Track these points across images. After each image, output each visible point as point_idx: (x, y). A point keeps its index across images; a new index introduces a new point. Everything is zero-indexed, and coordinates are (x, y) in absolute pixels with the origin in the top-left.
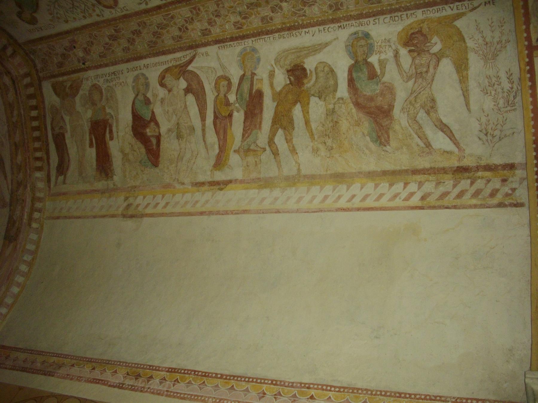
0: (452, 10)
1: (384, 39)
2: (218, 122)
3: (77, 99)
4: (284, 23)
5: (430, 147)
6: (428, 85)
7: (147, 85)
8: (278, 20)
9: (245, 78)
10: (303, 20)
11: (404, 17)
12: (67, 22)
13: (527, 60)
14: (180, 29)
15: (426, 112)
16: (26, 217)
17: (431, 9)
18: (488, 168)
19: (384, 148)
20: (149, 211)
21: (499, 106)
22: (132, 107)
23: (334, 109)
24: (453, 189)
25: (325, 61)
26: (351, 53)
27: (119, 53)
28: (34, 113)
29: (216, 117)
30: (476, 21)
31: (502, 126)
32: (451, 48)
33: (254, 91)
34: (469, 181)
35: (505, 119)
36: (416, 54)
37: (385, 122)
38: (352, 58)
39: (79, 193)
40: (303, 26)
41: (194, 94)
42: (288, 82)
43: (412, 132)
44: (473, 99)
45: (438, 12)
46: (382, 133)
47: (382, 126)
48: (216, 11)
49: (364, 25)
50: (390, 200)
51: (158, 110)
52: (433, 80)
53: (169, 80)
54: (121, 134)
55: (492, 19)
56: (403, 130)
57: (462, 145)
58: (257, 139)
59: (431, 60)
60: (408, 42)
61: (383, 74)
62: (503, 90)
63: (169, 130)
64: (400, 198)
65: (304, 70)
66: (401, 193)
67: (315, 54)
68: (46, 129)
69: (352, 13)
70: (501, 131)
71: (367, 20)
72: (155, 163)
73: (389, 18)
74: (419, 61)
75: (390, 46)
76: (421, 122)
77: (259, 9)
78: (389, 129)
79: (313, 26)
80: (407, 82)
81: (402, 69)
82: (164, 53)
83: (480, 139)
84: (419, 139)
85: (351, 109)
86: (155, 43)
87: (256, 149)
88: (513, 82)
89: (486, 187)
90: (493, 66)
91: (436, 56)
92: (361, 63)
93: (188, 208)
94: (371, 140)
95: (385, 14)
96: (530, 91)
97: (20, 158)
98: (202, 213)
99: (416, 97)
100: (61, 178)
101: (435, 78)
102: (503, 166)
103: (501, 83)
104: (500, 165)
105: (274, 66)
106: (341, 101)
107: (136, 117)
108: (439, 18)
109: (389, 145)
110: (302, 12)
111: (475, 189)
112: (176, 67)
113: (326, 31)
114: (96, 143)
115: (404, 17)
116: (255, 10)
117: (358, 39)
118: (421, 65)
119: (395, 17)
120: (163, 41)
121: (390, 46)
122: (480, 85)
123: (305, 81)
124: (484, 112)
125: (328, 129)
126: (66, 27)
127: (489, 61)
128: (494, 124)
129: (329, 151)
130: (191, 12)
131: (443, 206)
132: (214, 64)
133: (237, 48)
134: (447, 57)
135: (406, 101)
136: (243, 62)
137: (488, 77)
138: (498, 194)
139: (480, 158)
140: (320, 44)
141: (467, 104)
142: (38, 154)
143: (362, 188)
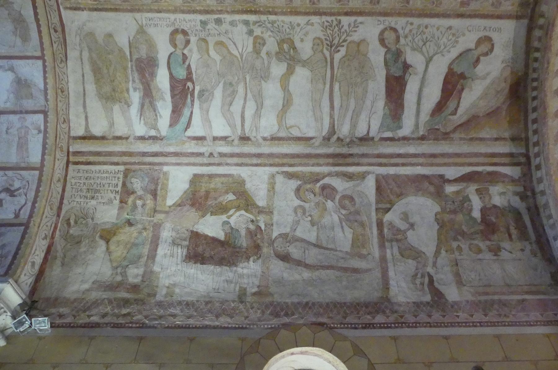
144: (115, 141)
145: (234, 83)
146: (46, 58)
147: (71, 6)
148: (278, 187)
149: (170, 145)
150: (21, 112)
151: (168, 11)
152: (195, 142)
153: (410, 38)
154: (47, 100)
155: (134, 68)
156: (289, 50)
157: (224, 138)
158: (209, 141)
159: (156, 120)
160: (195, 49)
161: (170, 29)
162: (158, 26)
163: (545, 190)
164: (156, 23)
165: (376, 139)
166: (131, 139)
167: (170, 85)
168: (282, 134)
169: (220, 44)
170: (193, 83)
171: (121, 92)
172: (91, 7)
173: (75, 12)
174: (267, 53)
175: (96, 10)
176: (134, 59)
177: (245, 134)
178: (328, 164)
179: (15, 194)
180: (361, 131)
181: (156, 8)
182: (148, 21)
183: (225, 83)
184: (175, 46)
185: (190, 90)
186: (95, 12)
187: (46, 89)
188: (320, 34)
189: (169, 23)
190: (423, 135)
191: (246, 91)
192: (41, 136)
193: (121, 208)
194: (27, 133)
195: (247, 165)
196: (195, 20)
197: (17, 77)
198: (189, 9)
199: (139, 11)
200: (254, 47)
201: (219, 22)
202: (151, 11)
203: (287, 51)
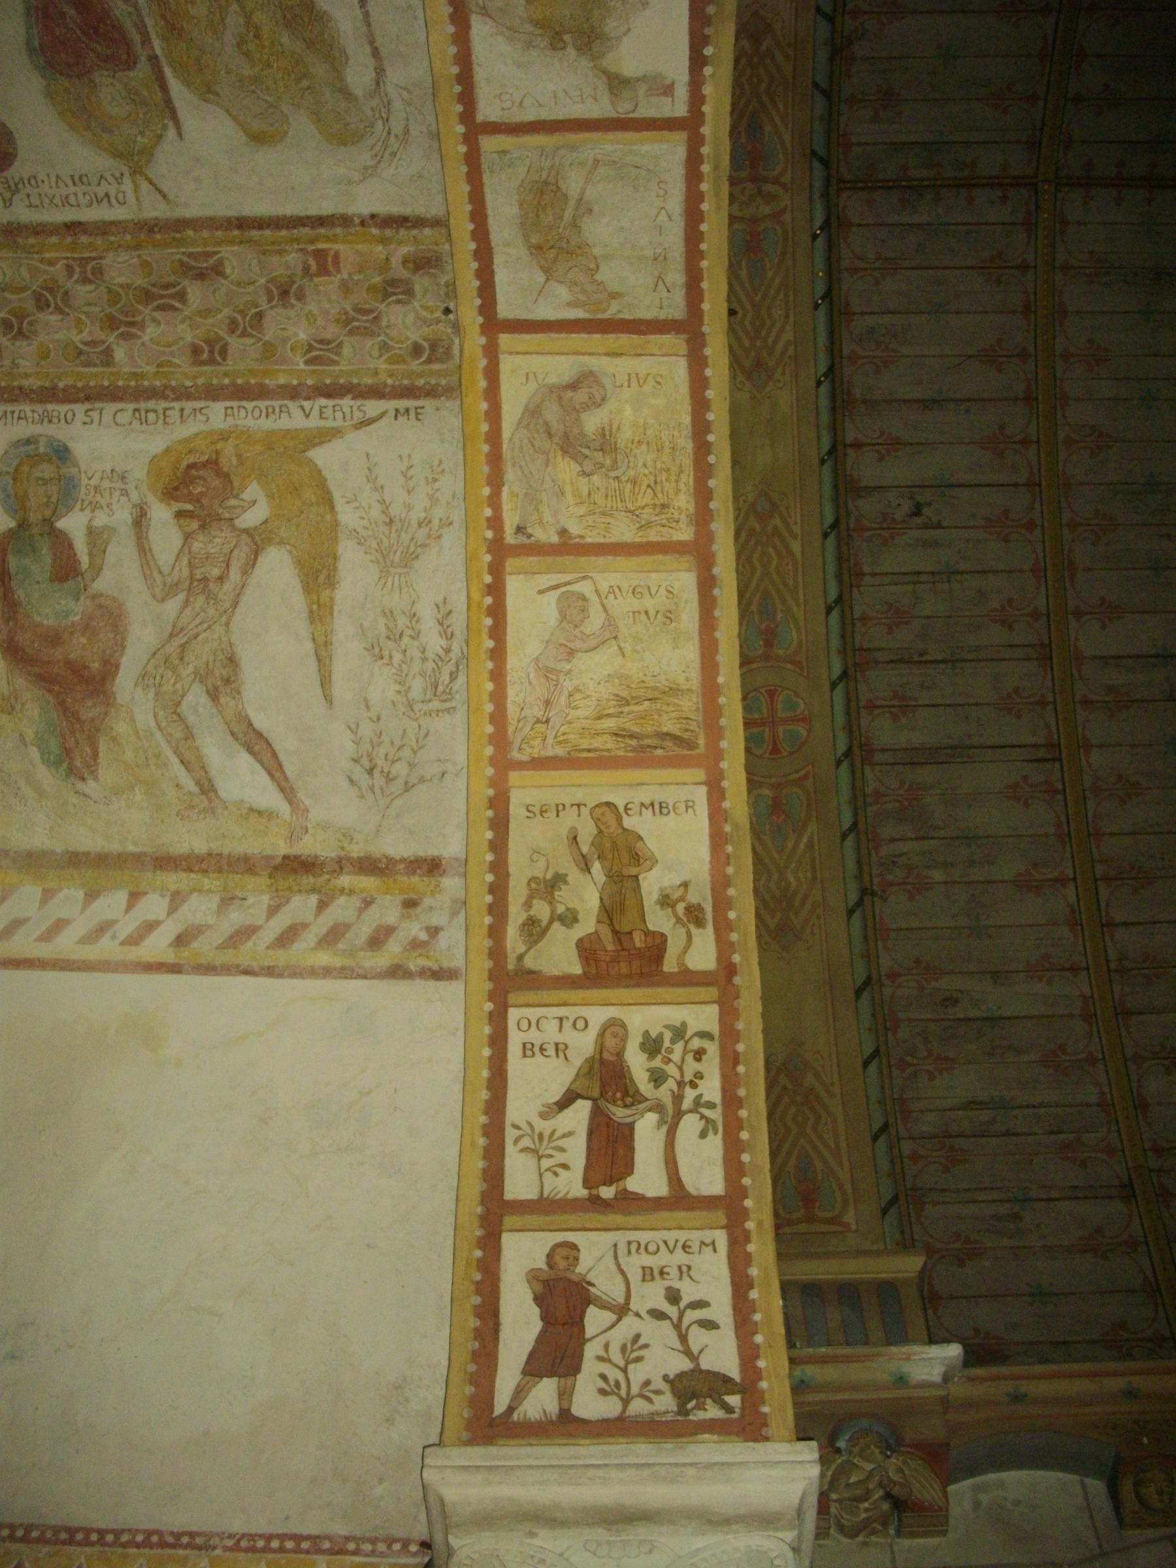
0: (307, 416)
1: (108, 468)
5: (212, 795)
6: (221, 615)
11: (174, 415)
13: (488, 579)
15: (208, 692)
17: (250, 405)
18: (369, 865)
19: (80, 786)
21: (411, 696)
24: (267, 920)
26: (8, 496)
30: (368, 455)
31: (415, 753)
32: (295, 520)
34: (314, 900)
35: (422, 733)
36: (195, 525)
37: (89, 710)
38: (11, 512)
44: (340, 670)
45: (267, 416)
46: (77, 742)
47: (78, 720)
49: (55, 420)
52: (235, 604)
55: (409, 456)
56: (138, 737)
57: (301, 795)
59: (235, 546)
60: (176, 489)
61: (98, 571)
62: (423, 652)
64: (114, 937)
66: (115, 922)
69: (25, 383)
70: (410, 765)
73: (130, 412)
74: (201, 545)
75: (125, 492)
76: (191, 719)
78: (98, 730)
80: (163, 600)
81: (152, 563)
83: (352, 782)
84: (183, 768)
88: (452, 635)
89: (359, 917)
90: (403, 584)
91: (251, 536)
92: (35, 530)
94: (42, 758)
95: (121, 399)
96: (490, 665)
99: (183, 647)
101: (244, 600)
102: (411, 862)
103: (419, 633)
104: (403, 860)
108: (270, 433)
109: (96, 779)
111: (331, 924)
115: (174, 415)
118: (207, 558)
119: (147, 412)
121: (125, 492)
124: (368, 707)
127: (392, 570)
128: (392, 743)
131: (238, 966)
134: (281, 543)
135: (155, 654)
137: (387, 611)
138: (391, 939)
139: (348, 836)
141: (325, 682)
146: (461, 129)
147: (415, 232)
151: (40, 230)
155: (136, 38)
162: (72, 177)
164: (79, 190)
172: (339, 231)
173: (407, 211)
175: (321, 221)
181: (84, 239)
182: (112, 195)
186: (324, 213)
189: (29, 189)
199: (150, 227)
202: (103, 229)
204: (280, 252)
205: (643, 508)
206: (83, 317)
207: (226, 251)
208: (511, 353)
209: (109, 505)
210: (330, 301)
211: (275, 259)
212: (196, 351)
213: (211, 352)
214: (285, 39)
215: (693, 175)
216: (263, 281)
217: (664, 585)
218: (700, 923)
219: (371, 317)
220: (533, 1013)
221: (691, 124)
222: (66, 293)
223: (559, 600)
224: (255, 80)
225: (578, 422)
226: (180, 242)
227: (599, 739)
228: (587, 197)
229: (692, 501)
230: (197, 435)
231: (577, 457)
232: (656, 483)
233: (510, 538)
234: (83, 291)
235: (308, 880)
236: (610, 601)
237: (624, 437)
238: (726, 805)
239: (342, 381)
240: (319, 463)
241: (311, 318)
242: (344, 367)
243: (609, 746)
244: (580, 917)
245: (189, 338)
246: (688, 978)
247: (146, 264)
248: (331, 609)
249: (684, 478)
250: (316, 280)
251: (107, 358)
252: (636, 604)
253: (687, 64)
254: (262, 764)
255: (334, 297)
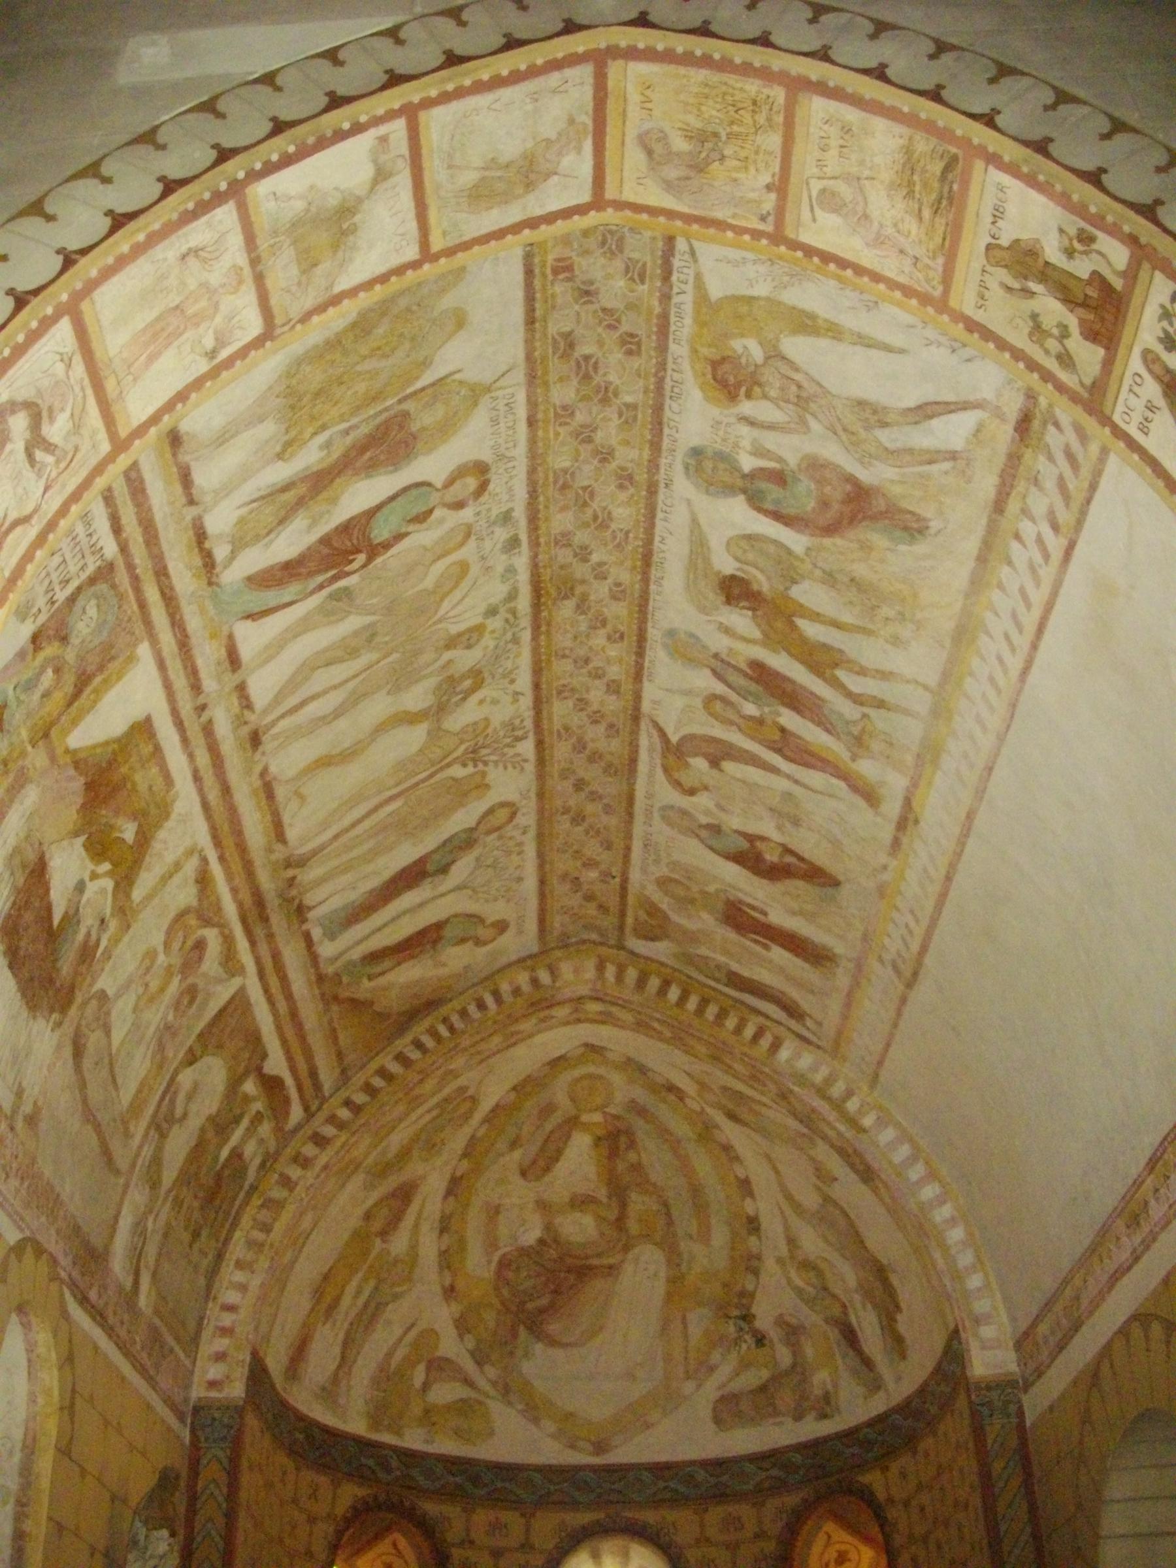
2: (789, 754)
3: (675, 917)
4: (634, 568)
7: (684, 813)
8: (626, 576)
9: (718, 670)
10: (636, 538)
11: (676, 376)
12: (520, 879)
14: (596, 722)
16: (842, 1128)
17: (673, 328)
20: (915, 946)
22: (719, 854)
23: (824, 571)
25: (725, 540)
27: (613, 821)
28: (674, 994)
29: (779, 751)
33: (749, 671)
36: (757, 389)
37: (880, 504)
39: (845, 1017)
40: (649, 541)
41: (723, 759)
42: (750, 613)
43: (911, 469)
48: (575, 662)
50: (1038, 584)
51: (734, 822)
52: (819, 384)
53: (688, 780)
54: (760, 895)
57: (971, 398)
58: (841, 715)
60: (730, 393)
61: (780, 460)
63: (779, 828)
65: (733, 577)
67: (709, 548)
68: (714, 989)
71: (665, 438)
72: (836, 884)
76: (899, 445)
77: (592, 598)
79: (652, 525)
82: (633, 761)
83: (969, 360)
85: (835, 545)
86: (610, 765)
87: (859, 728)
93: (934, 889)
97: (738, 1066)
98: (948, 878)
99: (845, 430)
100: (809, 1022)
105: (709, 618)
106: (814, 554)
107: (738, 858)
109: (930, 520)
110: (620, 535)
112: (664, 757)
113: (668, 509)
114: (765, 937)
115: (676, 376)
116: (592, 604)
117: (699, 469)
120: (612, 754)
122: (853, 308)
123: (755, 587)
124: (912, 327)
125: (122, 1323)
126: (530, 884)
129: (904, 620)
130: (566, 698)
132: (679, 702)
133: (658, 656)
136: (690, 660)
140: (692, 532)
141: (888, 348)
142: (749, 1031)
143: (997, 614)
144: (176, 476)
145: (378, 639)
146: (426, 267)
148: (177, 879)
149: (203, 611)
150: (255, 262)
151: (532, 441)
152: (223, 652)
153: (498, 844)
154: (306, 318)
155: (385, 415)
156: (460, 693)
157: (246, 703)
158: (231, 680)
159: (257, 538)
160: (448, 525)
161: (486, 456)
163: (296, 1184)
164: (502, 420)
165: (304, 927)
166: (192, 512)
167: (352, 518)
168: (280, 792)
169: (464, 567)
170: (364, 566)
171: (313, 418)
172: (536, 260)
174: (450, 661)
175: (529, 272)
176: (404, 406)
177: (265, 734)
178: (240, 905)
179: (39, 455)
180: (309, 899)
181: (540, 416)
182: (506, 401)
183: (372, 625)
184: (450, 483)
185: (347, 569)
187: (335, 300)
188: (496, 721)
190: (326, 975)
191: (361, 673)
192: (204, 366)
193: (21, 655)
194: (197, 320)
195: (201, 791)
196: (511, 498)
197: (360, 200)
198: (541, 482)
200: (460, 635)
201: (513, 544)
202: (532, 404)
203: (458, 689)
204: (553, 296)
205: (755, 121)
206: (601, 416)
207: (552, 329)
208: (621, 192)
209: (737, 437)
210: (594, 263)
211: (559, 301)
212: (630, 353)
213: (630, 343)
214: (380, 331)
215: (460, 93)
216: (577, 307)
217: (820, 124)
218: (1092, 239)
219: (609, 236)
220: (1120, 408)
221: (410, 112)
222: (581, 426)
223: (823, 209)
224: (413, 339)
225: (678, 154)
226: (544, 359)
227: (937, 226)
228: (483, 165)
229: (751, 80)
230: (693, 367)
231: (708, 162)
232: (733, 106)
233: (768, 227)
234: (580, 418)
235: (1036, 424)
236: (828, 171)
237: (696, 123)
238: (1007, 158)
239: (659, 262)
240: (720, 295)
241: (608, 277)
242: (648, 259)
243: (943, 221)
244: (1065, 323)
245: (620, 356)
246: (1131, 274)
247: (561, 379)
248: (832, 323)
249: (731, 82)
250: (577, 272)
251: (633, 407)
252: (834, 152)
253: (359, 136)
254: (940, 414)
255: (592, 260)
